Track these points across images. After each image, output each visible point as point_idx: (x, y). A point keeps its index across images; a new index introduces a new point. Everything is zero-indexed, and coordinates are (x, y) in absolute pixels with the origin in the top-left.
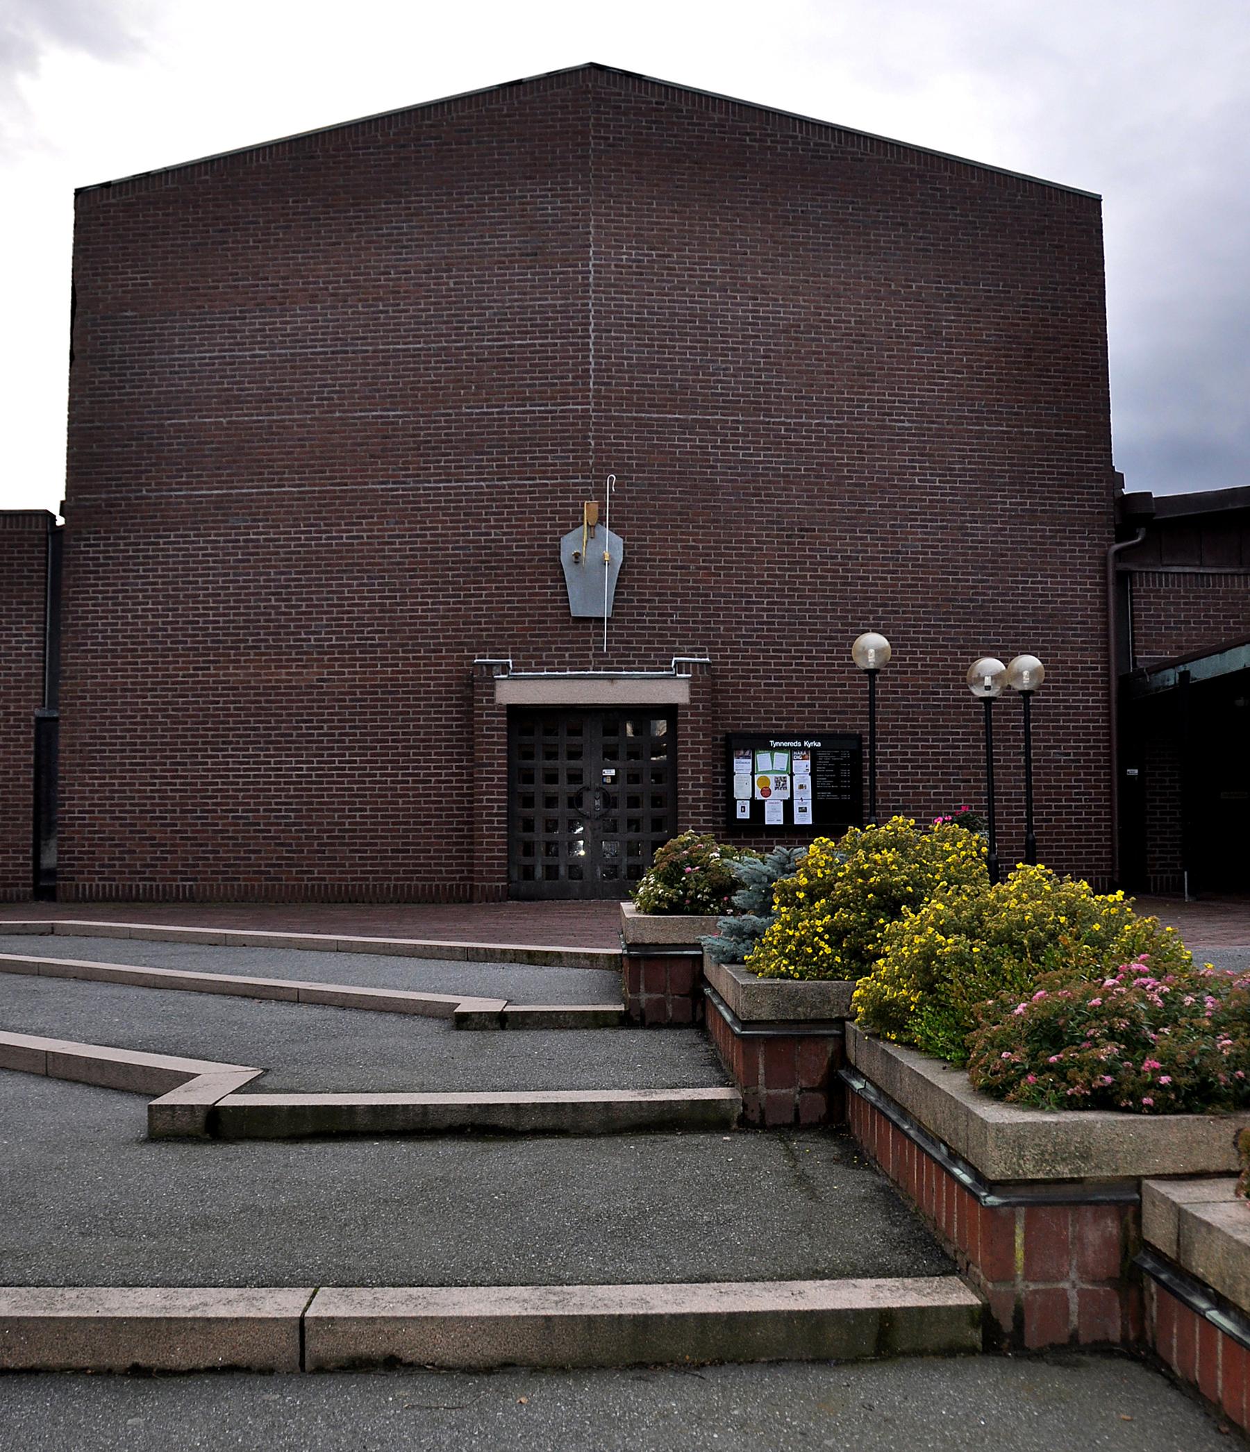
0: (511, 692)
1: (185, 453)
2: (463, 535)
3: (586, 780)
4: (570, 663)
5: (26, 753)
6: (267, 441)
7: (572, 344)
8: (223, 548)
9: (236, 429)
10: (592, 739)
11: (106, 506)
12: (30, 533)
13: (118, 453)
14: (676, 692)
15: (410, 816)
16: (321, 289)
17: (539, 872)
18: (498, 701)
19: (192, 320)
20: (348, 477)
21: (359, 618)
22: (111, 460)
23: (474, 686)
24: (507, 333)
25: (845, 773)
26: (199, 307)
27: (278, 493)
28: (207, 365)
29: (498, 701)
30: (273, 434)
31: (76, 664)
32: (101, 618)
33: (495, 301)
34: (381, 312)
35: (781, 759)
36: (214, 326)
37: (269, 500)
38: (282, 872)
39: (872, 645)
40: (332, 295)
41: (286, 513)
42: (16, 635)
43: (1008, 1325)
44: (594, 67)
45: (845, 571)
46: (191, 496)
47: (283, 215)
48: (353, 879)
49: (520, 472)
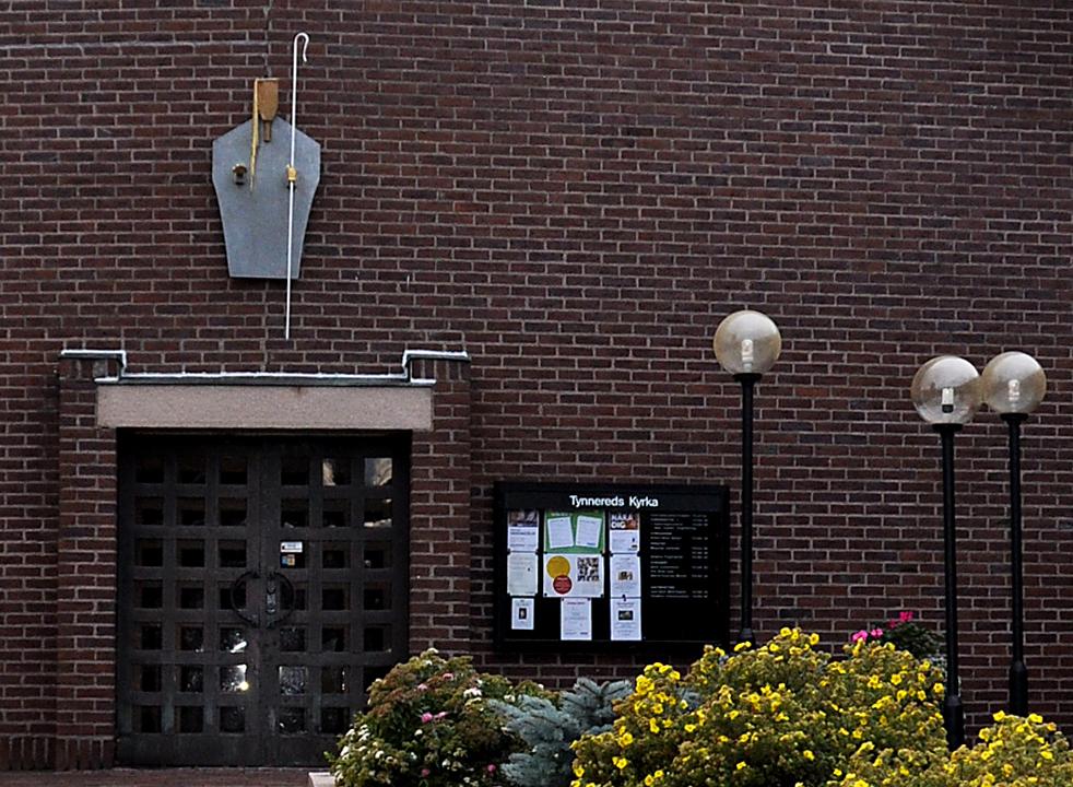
0: (126, 406)
2: (45, 134)
4: (226, 358)
10: (263, 489)
14: (409, 410)
17: (169, 718)
18: (101, 422)
23: (60, 395)
25: (699, 553)
29: (101, 422)
35: (590, 528)
39: (749, 332)
49: (143, 27)
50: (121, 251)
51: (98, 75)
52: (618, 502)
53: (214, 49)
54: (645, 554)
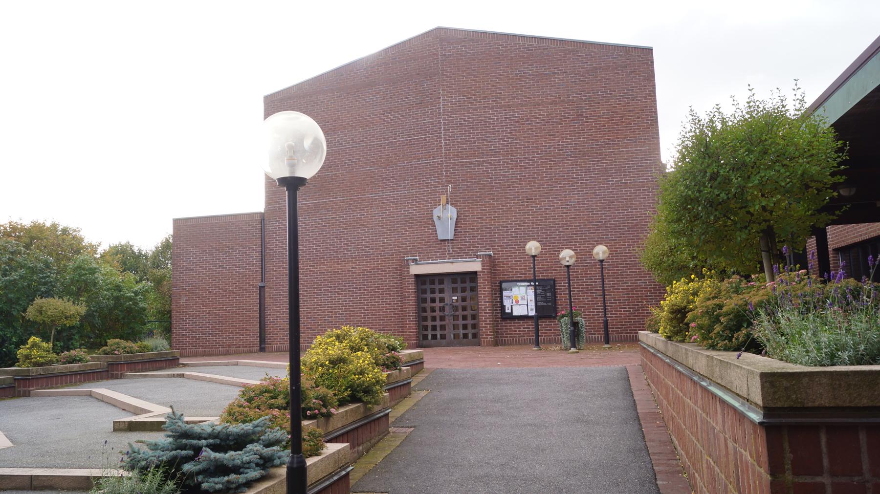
0: (415, 270)
10: (447, 286)
14: (475, 266)
17: (430, 337)
23: (405, 266)
35: (523, 289)
43: (261, 462)
44: (439, 30)
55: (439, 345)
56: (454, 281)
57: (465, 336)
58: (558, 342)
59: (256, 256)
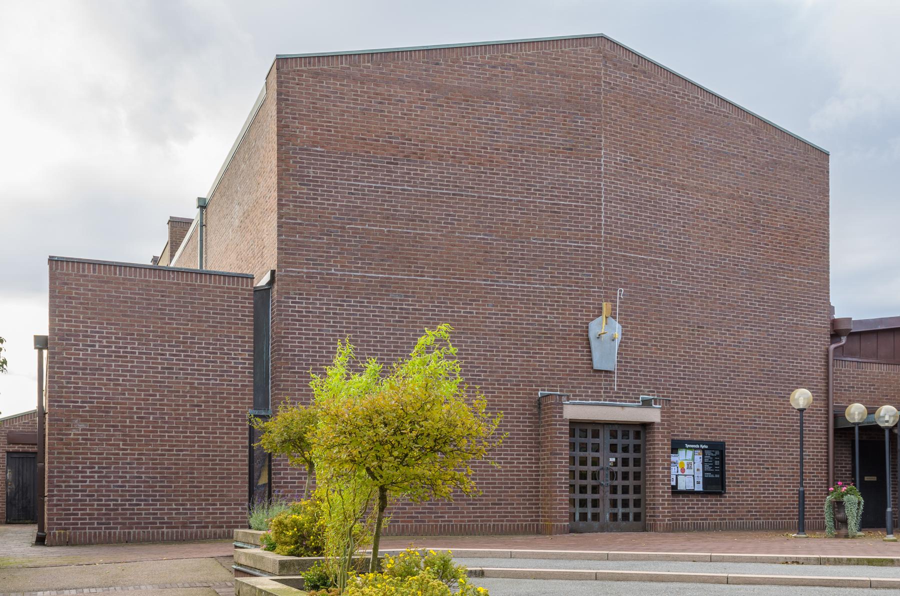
0: (573, 411)
1: (359, 247)
2: (532, 316)
3: (601, 465)
4: (591, 396)
5: (242, 438)
6: (413, 246)
7: (592, 208)
8: (386, 312)
9: (394, 236)
11: (307, 277)
12: (242, 289)
13: (313, 243)
14: (653, 415)
15: (502, 483)
16: (445, 152)
18: (565, 417)
19: (362, 160)
20: (464, 275)
21: (472, 363)
22: (310, 247)
24: (556, 196)
25: (717, 463)
26: (367, 152)
27: (421, 280)
28: (373, 191)
29: (565, 417)
30: (416, 242)
31: (288, 381)
32: (305, 351)
33: (550, 175)
34: (482, 172)
35: (690, 453)
36: (377, 166)
37: (415, 284)
38: (425, 517)
40: (452, 157)
41: (426, 293)
42: (234, 359)
45: (718, 351)
46: (365, 276)
47: (420, 99)
48: (469, 521)
49: (563, 282)
50: (557, 358)
51: (549, 297)
52: (698, 446)
53: (586, 291)
54: (703, 463)
55: (590, 530)
56: (614, 435)
57: (625, 516)
58: (822, 528)
59: (243, 357)
